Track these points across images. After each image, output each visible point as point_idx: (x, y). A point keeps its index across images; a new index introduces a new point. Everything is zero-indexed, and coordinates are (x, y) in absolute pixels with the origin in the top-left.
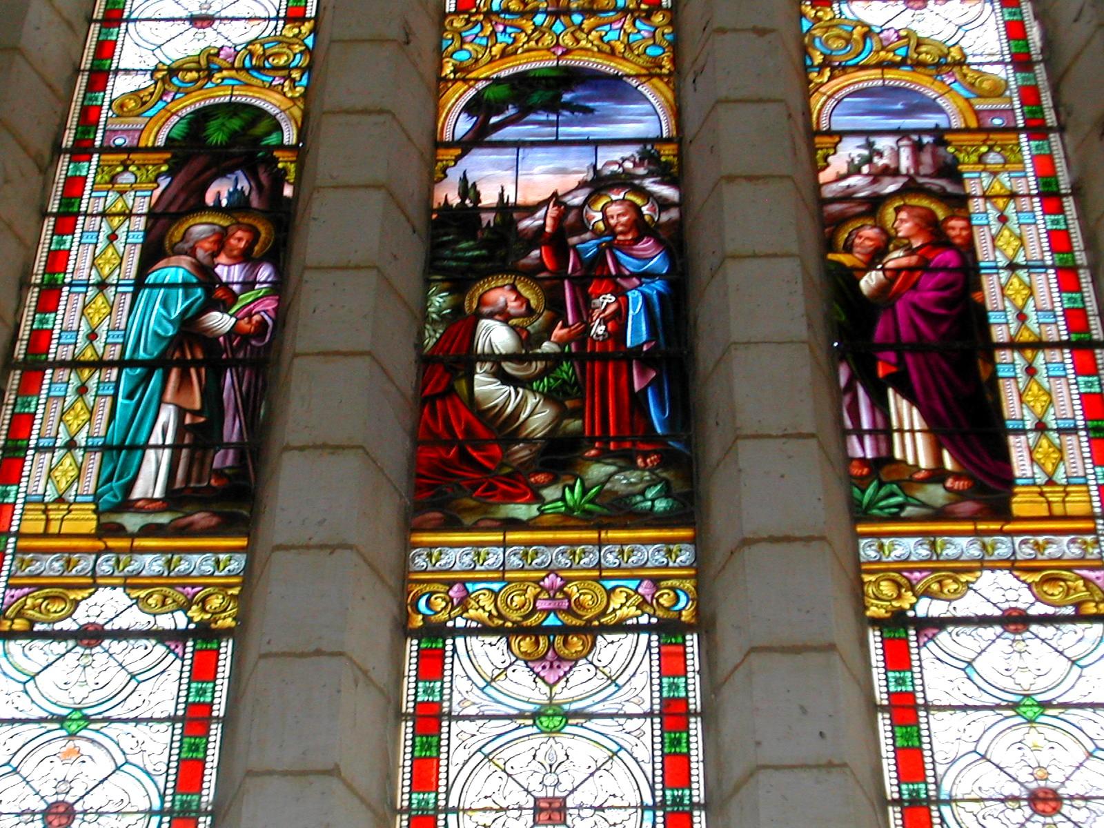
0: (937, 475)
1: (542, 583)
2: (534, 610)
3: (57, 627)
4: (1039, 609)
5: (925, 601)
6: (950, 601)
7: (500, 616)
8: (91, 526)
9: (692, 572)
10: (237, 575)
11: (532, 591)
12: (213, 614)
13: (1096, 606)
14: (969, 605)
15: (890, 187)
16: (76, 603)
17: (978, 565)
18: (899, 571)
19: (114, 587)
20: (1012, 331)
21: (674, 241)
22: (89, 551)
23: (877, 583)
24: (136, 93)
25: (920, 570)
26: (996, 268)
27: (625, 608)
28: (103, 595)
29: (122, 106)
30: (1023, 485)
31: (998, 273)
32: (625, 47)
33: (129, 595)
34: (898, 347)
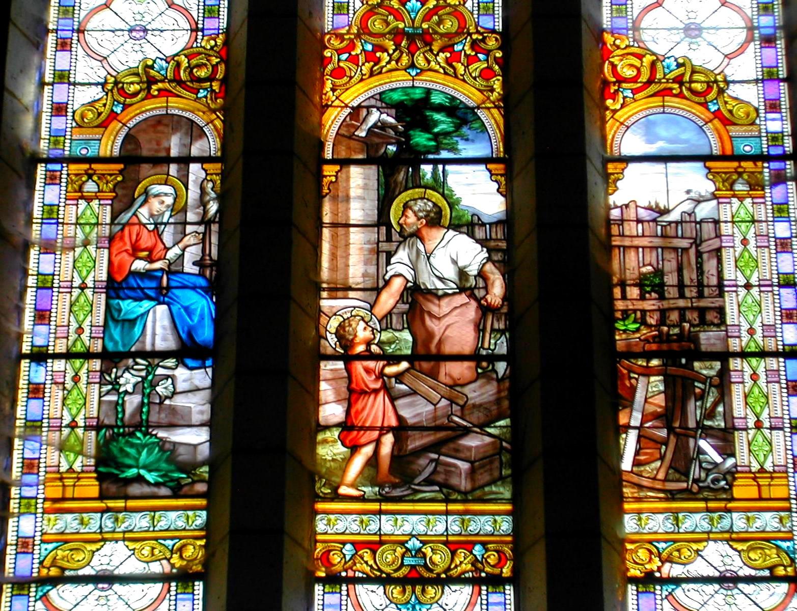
3: (81, 573)
4: (746, 572)
5: (667, 565)
7: (379, 570)
8: (94, 491)
9: (203, 533)
10: (509, 535)
11: (400, 551)
12: (188, 561)
13: (785, 570)
14: (699, 568)
17: (705, 536)
18: (650, 542)
19: (117, 541)
20: (743, 344)
22: (95, 510)
23: (635, 551)
24: (92, 103)
25: (666, 541)
26: (736, 286)
28: (109, 547)
29: (83, 117)
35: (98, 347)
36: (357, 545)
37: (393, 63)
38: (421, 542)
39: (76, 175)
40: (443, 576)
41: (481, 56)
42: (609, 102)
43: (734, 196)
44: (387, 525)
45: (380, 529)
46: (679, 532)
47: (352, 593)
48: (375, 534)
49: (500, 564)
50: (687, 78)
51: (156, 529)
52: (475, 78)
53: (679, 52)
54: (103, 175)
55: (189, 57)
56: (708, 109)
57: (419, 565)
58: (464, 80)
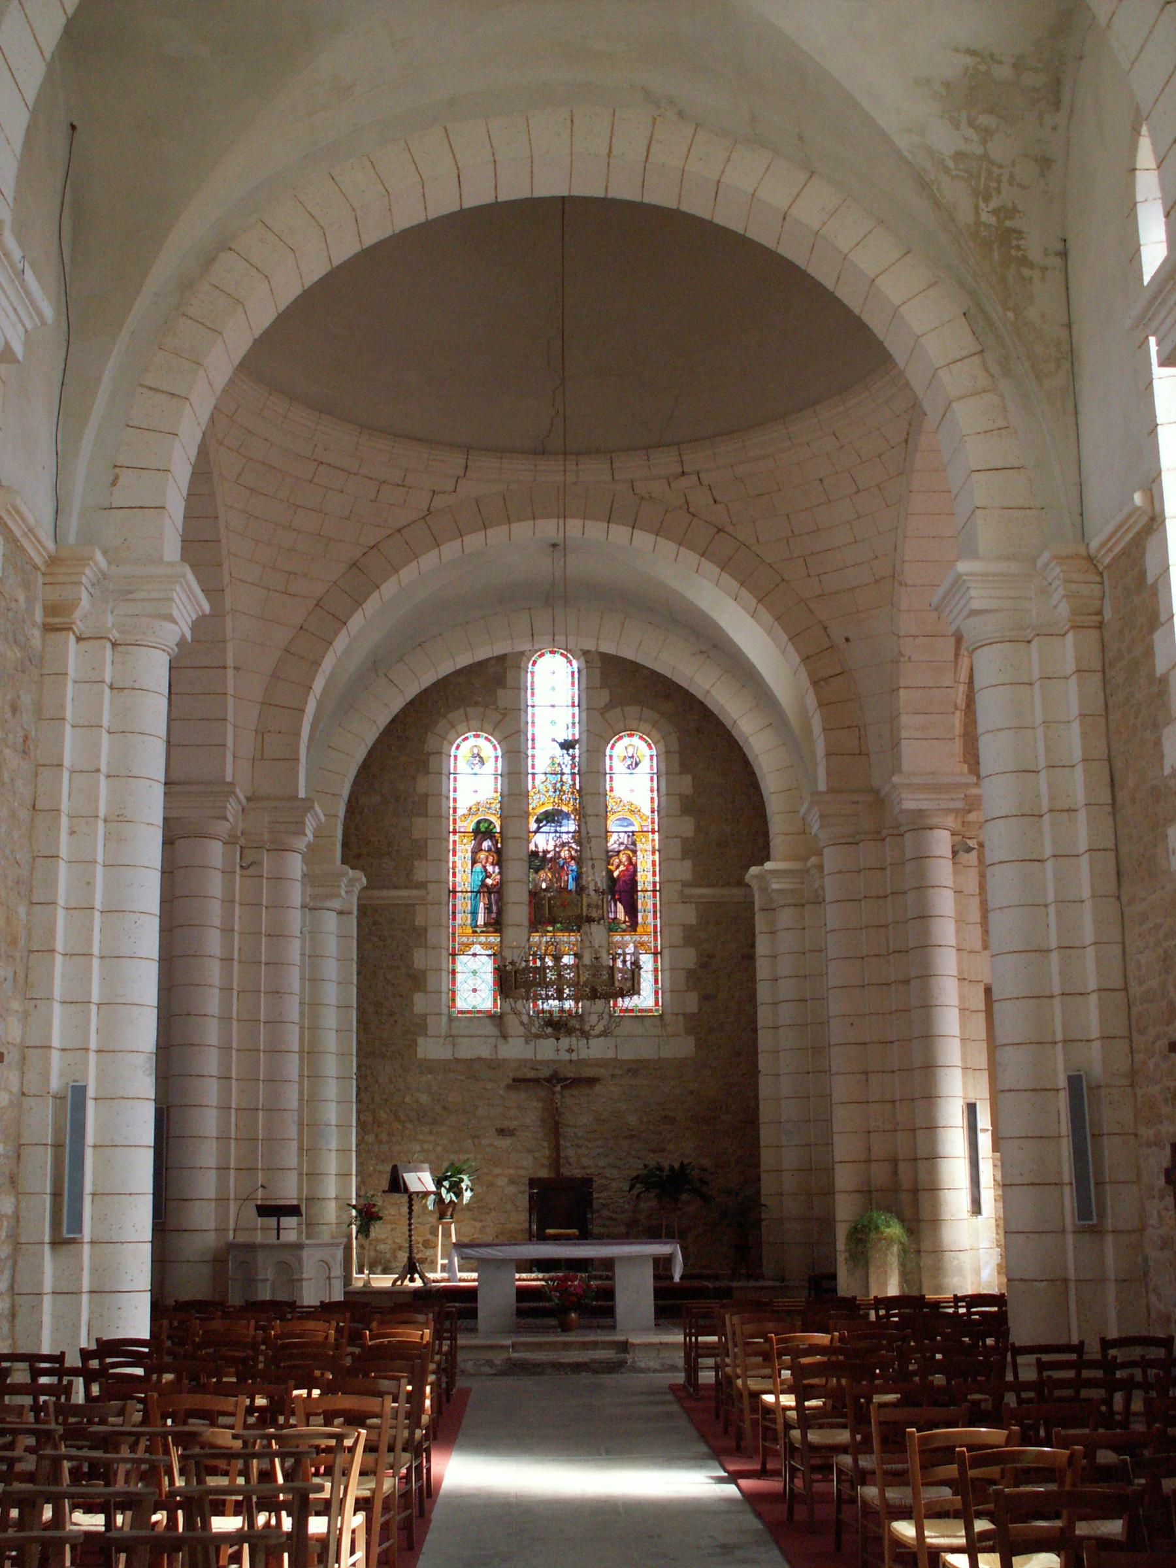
0: (625, 922)
15: (622, 848)
21: (579, 860)
34: (620, 892)
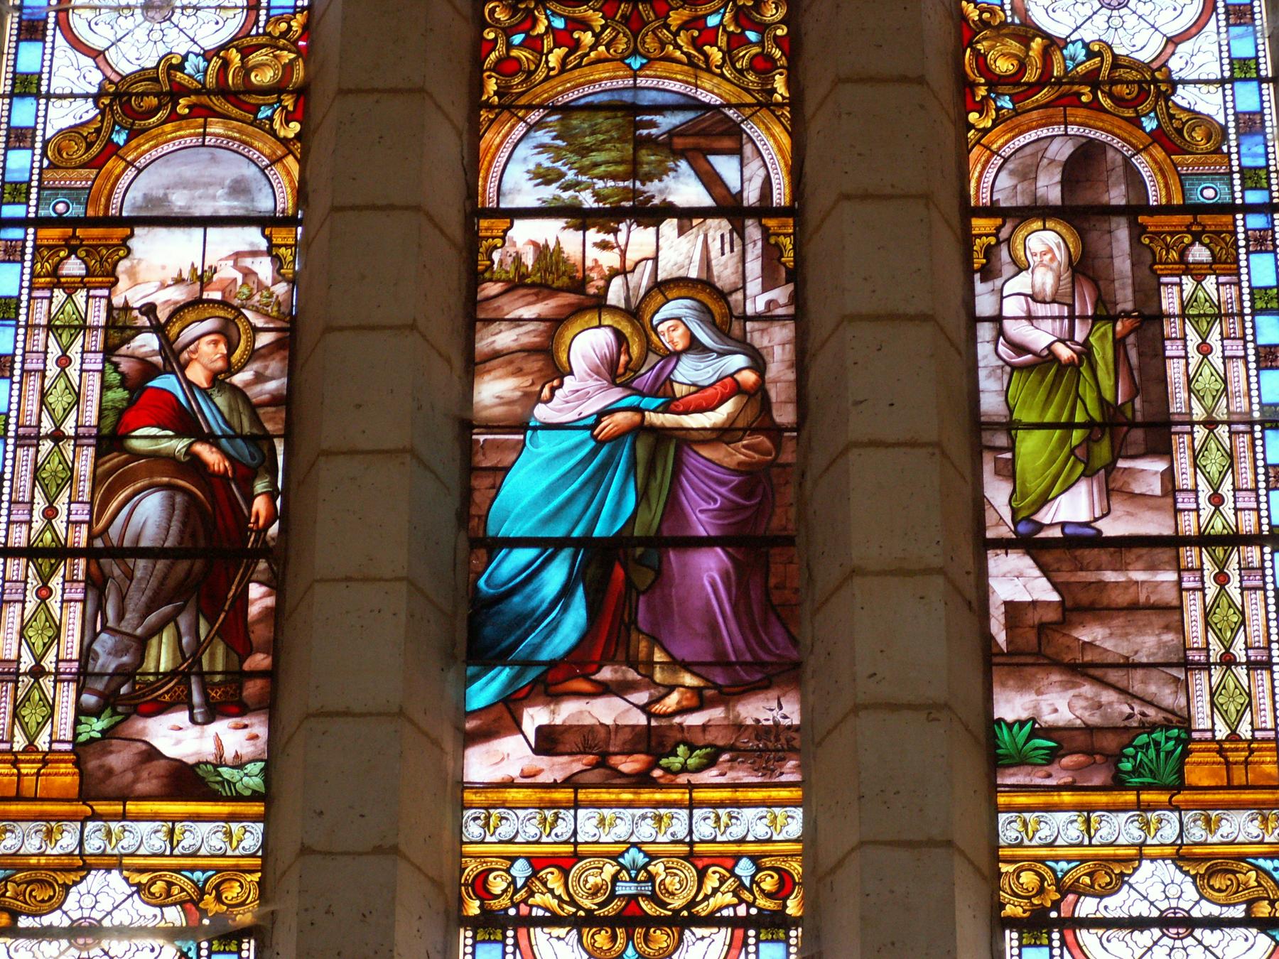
1: (621, 860)
2: (613, 896)
4: (1207, 909)
6: (1101, 897)
7: (573, 902)
10: (253, 856)
11: (610, 870)
12: (229, 906)
16: (67, 888)
18: (1042, 860)
22: (71, 818)
23: (1018, 874)
27: (719, 894)
28: (95, 879)
30: (1200, 741)
31: (1192, 433)
32: (723, 58)
33: (126, 879)
35: (81, 538)
36: (537, 863)
37: (602, 48)
38: (646, 854)
39: (49, 247)
40: (685, 913)
41: (752, 36)
42: (973, 117)
43: (1187, 272)
44: (587, 824)
45: (575, 833)
46: (1090, 845)
47: (523, 943)
48: (566, 842)
49: (781, 893)
50: (1104, 73)
51: (176, 852)
52: (741, 72)
53: (1088, 34)
54: (95, 247)
55: (245, 52)
56: (1143, 129)
57: (643, 895)
58: (722, 76)
